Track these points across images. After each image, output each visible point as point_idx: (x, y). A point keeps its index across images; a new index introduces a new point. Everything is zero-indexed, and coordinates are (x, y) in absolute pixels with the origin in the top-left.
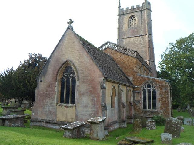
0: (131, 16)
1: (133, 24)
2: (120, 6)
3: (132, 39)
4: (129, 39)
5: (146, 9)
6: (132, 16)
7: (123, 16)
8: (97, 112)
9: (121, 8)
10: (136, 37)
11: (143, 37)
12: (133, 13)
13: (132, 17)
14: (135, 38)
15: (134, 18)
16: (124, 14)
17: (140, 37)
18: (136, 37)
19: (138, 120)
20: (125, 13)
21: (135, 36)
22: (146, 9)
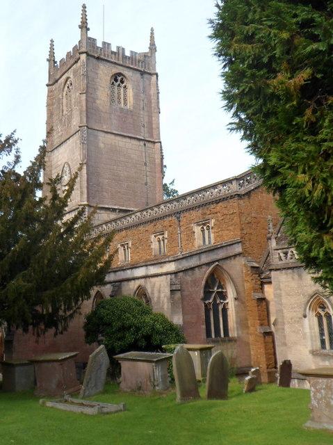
0: (117, 74)
1: (119, 98)
2: (84, 26)
3: (121, 142)
4: (113, 136)
5: (86, 53)
6: (120, 74)
7: (95, 61)
8: (95, 327)
9: (90, 34)
10: (130, 138)
11: (147, 144)
12: (125, 69)
13: (119, 78)
14: (128, 140)
15: (122, 82)
16: (98, 58)
17: (142, 143)
18: (130, 138)
19: (295, 103)
20: (102, 57)
21: (130, 135)
22: (86, 53)
